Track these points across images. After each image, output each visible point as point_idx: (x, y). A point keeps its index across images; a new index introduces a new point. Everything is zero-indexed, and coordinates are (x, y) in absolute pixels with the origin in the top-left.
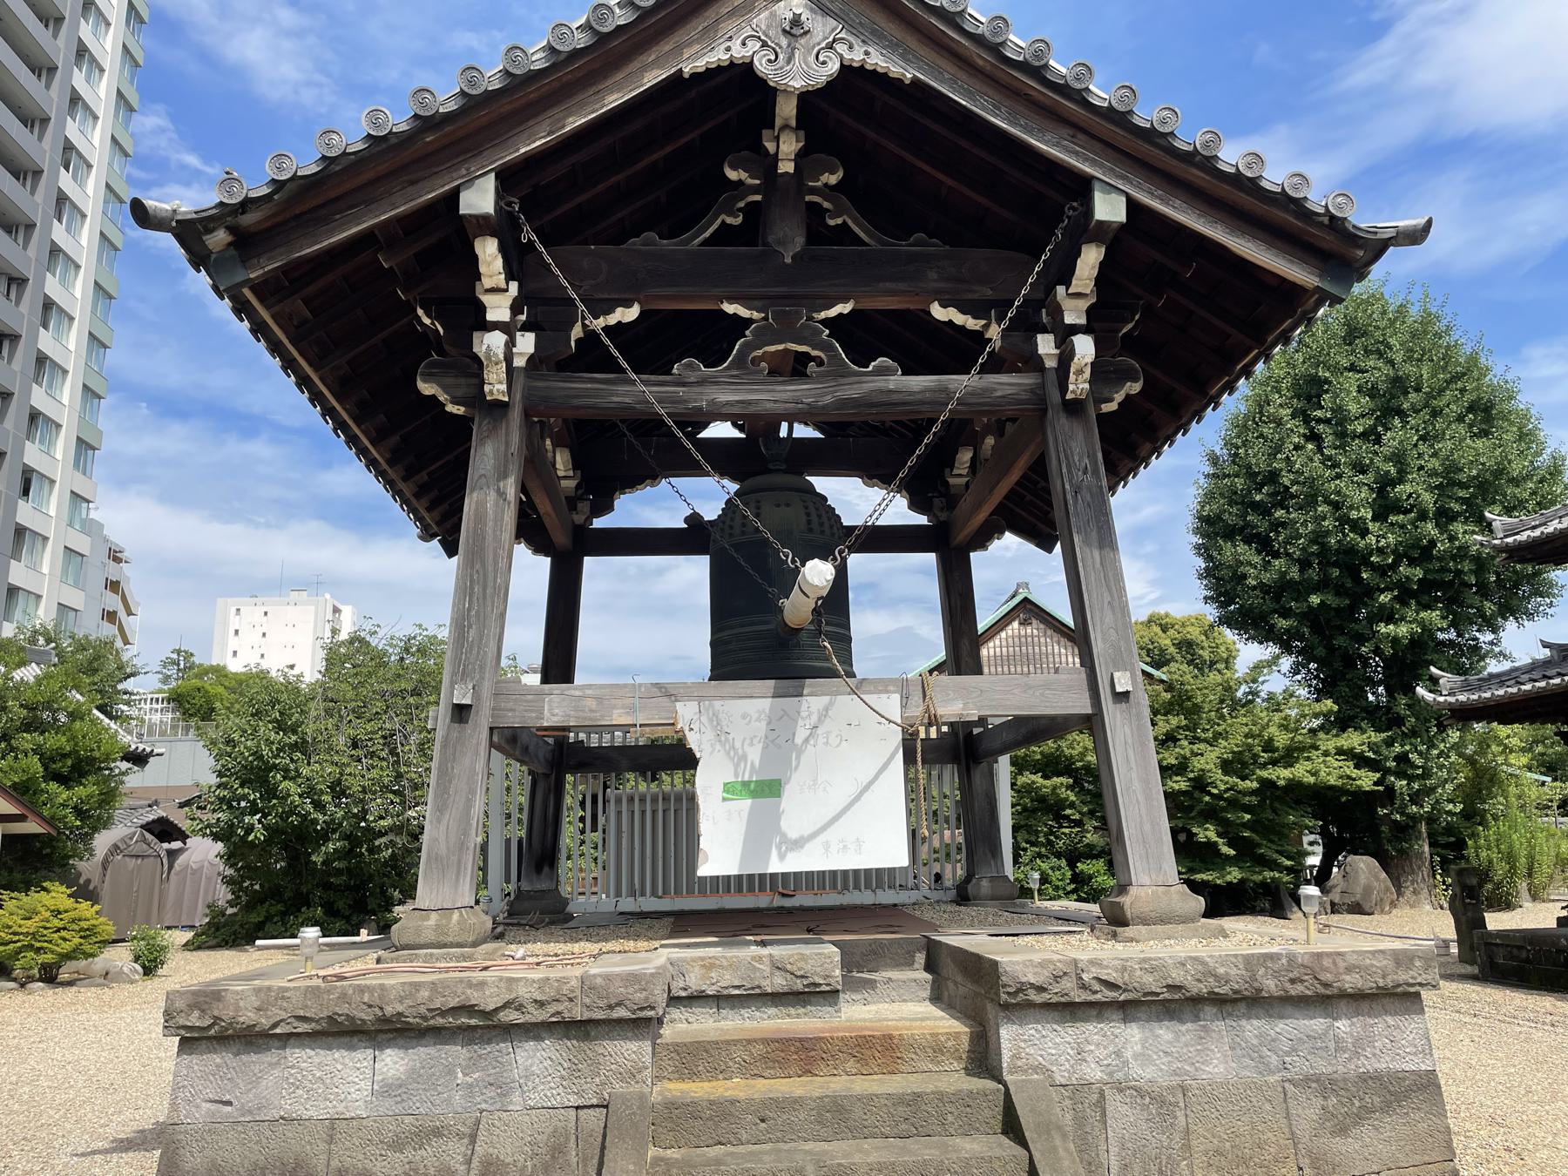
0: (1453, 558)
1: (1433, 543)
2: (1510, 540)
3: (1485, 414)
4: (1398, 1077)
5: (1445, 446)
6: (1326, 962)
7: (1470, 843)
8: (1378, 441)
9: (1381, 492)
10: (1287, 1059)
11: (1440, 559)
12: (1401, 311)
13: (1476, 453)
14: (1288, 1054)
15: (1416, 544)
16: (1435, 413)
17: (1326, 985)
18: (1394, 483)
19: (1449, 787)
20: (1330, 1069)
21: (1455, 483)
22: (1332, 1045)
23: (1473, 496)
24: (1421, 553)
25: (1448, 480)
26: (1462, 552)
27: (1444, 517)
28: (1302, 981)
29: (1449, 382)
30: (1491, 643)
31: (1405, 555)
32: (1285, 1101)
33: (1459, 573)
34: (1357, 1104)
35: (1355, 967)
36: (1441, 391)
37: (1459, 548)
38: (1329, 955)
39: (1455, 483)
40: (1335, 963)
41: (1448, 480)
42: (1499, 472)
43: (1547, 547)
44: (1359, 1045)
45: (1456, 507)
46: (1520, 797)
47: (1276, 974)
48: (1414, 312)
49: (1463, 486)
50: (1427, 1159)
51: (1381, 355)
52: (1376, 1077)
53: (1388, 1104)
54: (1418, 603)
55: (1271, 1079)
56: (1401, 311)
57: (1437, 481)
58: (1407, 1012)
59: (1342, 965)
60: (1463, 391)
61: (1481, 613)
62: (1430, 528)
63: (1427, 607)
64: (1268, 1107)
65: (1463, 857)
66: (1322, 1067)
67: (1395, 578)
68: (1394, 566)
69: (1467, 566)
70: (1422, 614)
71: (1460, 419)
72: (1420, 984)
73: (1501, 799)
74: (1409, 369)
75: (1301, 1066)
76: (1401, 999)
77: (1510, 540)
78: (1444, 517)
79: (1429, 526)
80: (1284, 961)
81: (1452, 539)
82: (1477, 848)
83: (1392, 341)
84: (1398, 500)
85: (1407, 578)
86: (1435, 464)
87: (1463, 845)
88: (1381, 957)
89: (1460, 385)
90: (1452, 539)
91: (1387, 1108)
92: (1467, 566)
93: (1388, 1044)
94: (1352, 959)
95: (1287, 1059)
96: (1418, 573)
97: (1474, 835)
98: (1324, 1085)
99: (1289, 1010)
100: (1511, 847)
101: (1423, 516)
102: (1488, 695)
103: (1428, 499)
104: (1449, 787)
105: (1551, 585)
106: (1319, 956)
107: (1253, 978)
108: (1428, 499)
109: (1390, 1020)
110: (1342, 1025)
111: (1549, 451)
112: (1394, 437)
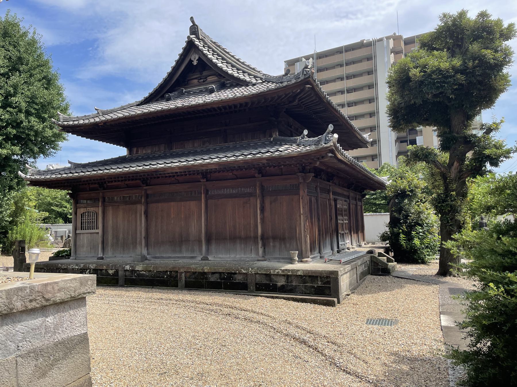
0: (28, 129)
1: (22, 122)
2: (66, 123)
3: (48, 82)
4: (70, 340)
5: (33, 88)
6: (49, 288)
7: (10, 232)
8: (8, 78)
9: (6, 98)
10: (20, 344)
11: (23, 128)
12: (25, 34)
13: (43, 95)
14: (20, 341)
15: (15, 121)
16: (31, 76)
17: (47, 300)
18: (11, 96)
19: (8, 211)
20: (41, 344)
21: (33, 102)
22: (43, 331)
23: (39, 109)
24: (17, 125)
25: (32, 100)
26: (31, 128)
27: (28, 114)
28: (35, 300)
29: (38, 66)
30: (33, 162)
31: (10, 124)
32: (16, 368)
33: (28, 135)
34: (52, 358)
35: (62, 288)
36: (35, 69)
37: (31, 126)
38: (50, 284)
39: (33, 102)
40: (53, 288)
41: (32, 100)
42: (49, 103)
43: (78, 129)
44: (56, 327)
45: (33, 111)
46: (30, 216)
47: (23, 299)
48: (30, 36)
49: (36, 104)
50: (79, 376)
51: (15, 47)
52: (62, 343)
53: (66, 354)
54: (11, 143)
55: (10, 358)
56: (25, 34)
57: (28, 100)
58: (79, 306)
59: (56, 288)
60: (42, 71)
61: (32, 150)
62: (22, 116)
63: (14, 145)
64: (6, 374)
65: (6, 237)
66: (37, 344)
67: (5, 132)
68: (6, 127)
69: (32, 133)
70: (13, 147)
71: (40, 80)
72: (84, 294)
73: (24, 217)
74: (24, 55)
75: (26, 346)
76: (78, 300)
77: (66, 123)
78: (28, 114)
79: (22, 115)
80: (28, 291)
81: (29, 122)
82: (12, 233)
83: (21, 43)
84: (11, 103)
85: (10, 133)
86: (28, 93)
87: (7, 233)
88: (74, 282)
89: (42, 68)
90: (29, 122)
91: (66, 356)
92: (32, 133)
93: (66, 325)
94: (61, 285)
95: (20, 344)
96: (14, 132)
97: (12, 230)
98: (36, 353)
99: (24, 317)
100: (25, 233)
101: (20, 111)
102: (48, 177)
103: (23, 105)
104: (8, 211)
105: (58, 145)
106: (46, 285)
107: (10, 303)
108: (23, 105)
109: (72, 312)
110: (50, 319)
111: (66, 101)
112: (15, 79)
